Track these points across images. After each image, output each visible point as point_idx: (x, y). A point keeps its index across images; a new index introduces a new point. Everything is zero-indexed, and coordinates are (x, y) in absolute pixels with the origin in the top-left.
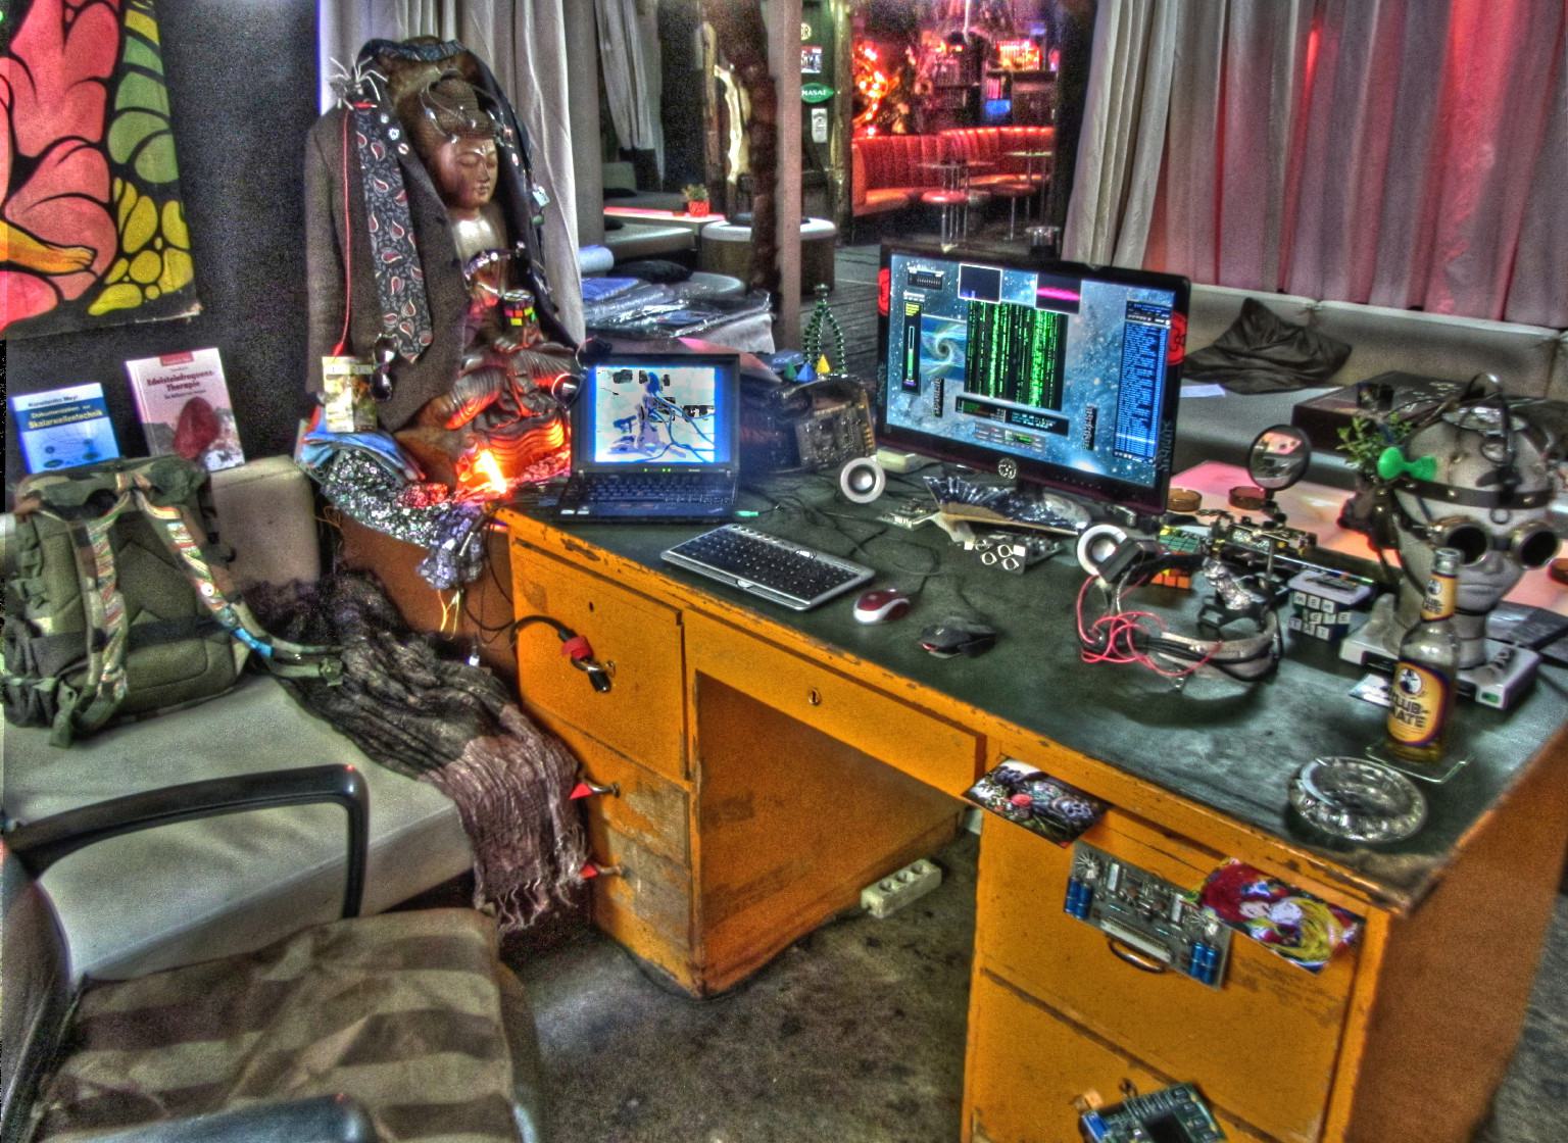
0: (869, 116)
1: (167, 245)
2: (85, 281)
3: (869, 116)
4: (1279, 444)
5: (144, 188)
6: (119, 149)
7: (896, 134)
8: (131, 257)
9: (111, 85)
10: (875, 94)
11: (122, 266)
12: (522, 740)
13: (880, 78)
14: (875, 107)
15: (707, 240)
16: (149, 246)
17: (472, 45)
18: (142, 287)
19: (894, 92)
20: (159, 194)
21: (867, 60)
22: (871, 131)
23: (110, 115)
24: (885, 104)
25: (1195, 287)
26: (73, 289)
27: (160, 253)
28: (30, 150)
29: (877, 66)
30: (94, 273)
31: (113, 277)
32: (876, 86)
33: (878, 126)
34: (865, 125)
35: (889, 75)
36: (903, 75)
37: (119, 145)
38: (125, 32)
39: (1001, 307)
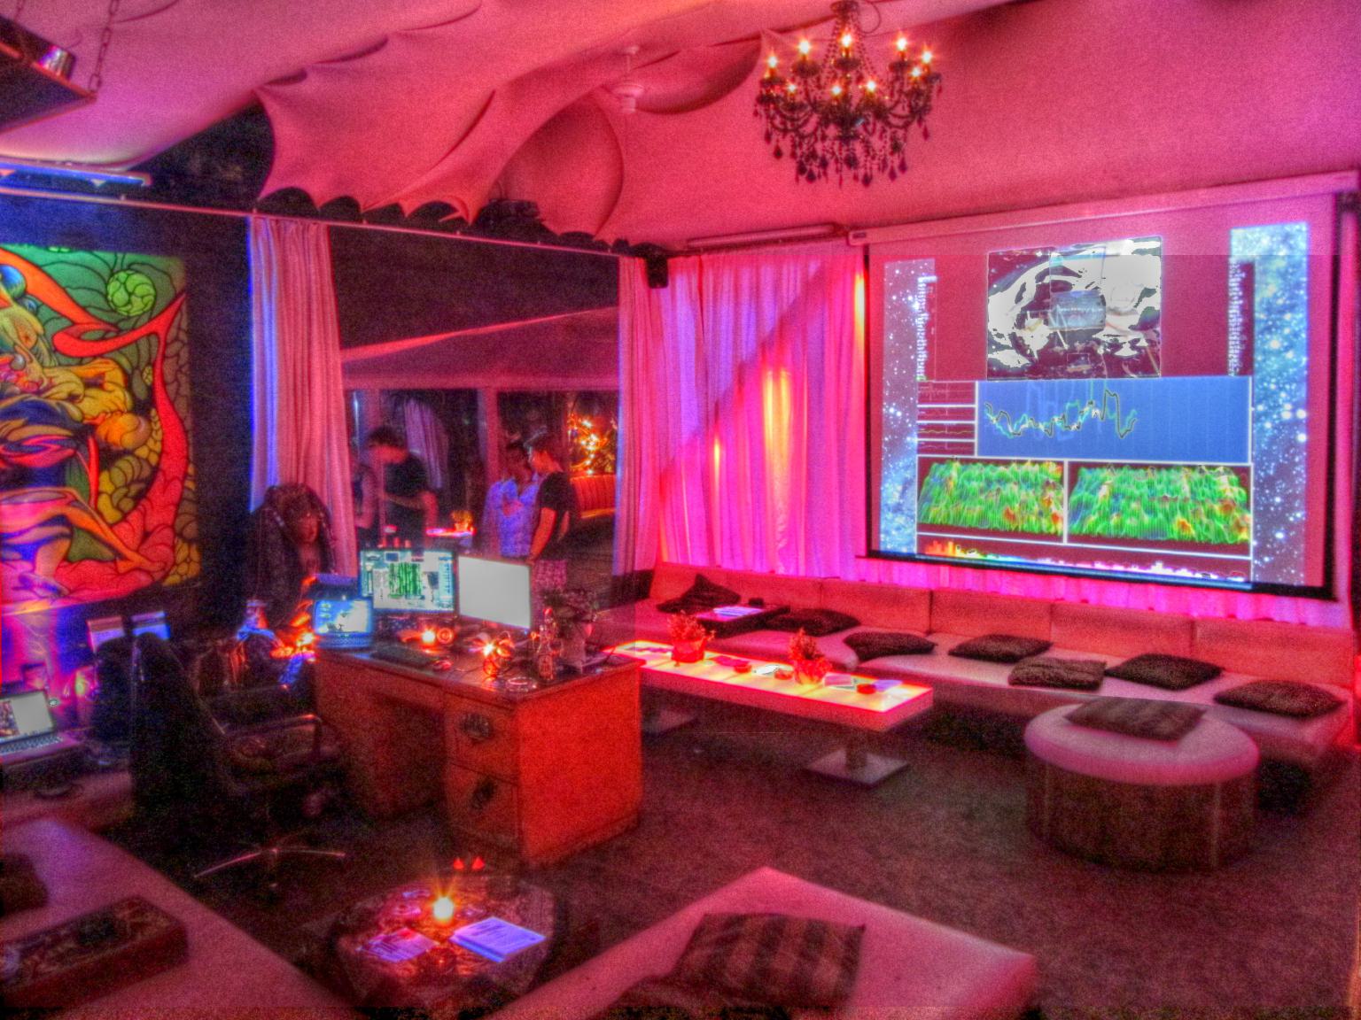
0: (588, 462)
1: (191, 560)
2: (162, 573)
3: (588, 462)
4: (1334, 896)
5: (185, 540)
6: (178, 528)
7: (608, 473)
8: (178, 565)
9: (178, 505)
10: (592, 448)
11: (175, 568)
12: (1090, 312)
13: (594, 438)
14: (592, 456)
15: (375, 627)
16: (185, 561)
17: (310, 485)
18: (181, 576)
19: (604, 447)
20: (190, 542)
21: (584, 427)
22: (590, 472)
23: (177, 515)
24: (599, 454)
25: (1250, 379)
26: (157, 576)
27: (188, 563)
28: (149, 528)
29: (593, 431)
30: (153, 578)
31: (172, 572)
32: (592, 443)
33: (595, 469)
34: (586, 468)
35: (601, 435)
36: (609, 437)
37: (179, 524)
38: (183, 487)
39: (969, 414)
